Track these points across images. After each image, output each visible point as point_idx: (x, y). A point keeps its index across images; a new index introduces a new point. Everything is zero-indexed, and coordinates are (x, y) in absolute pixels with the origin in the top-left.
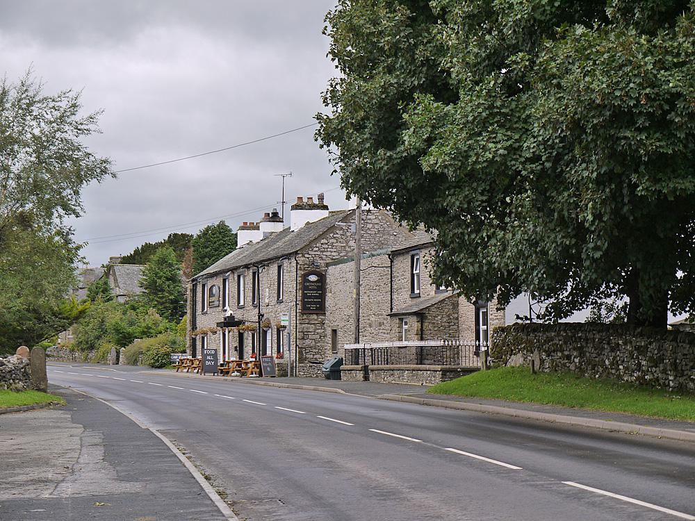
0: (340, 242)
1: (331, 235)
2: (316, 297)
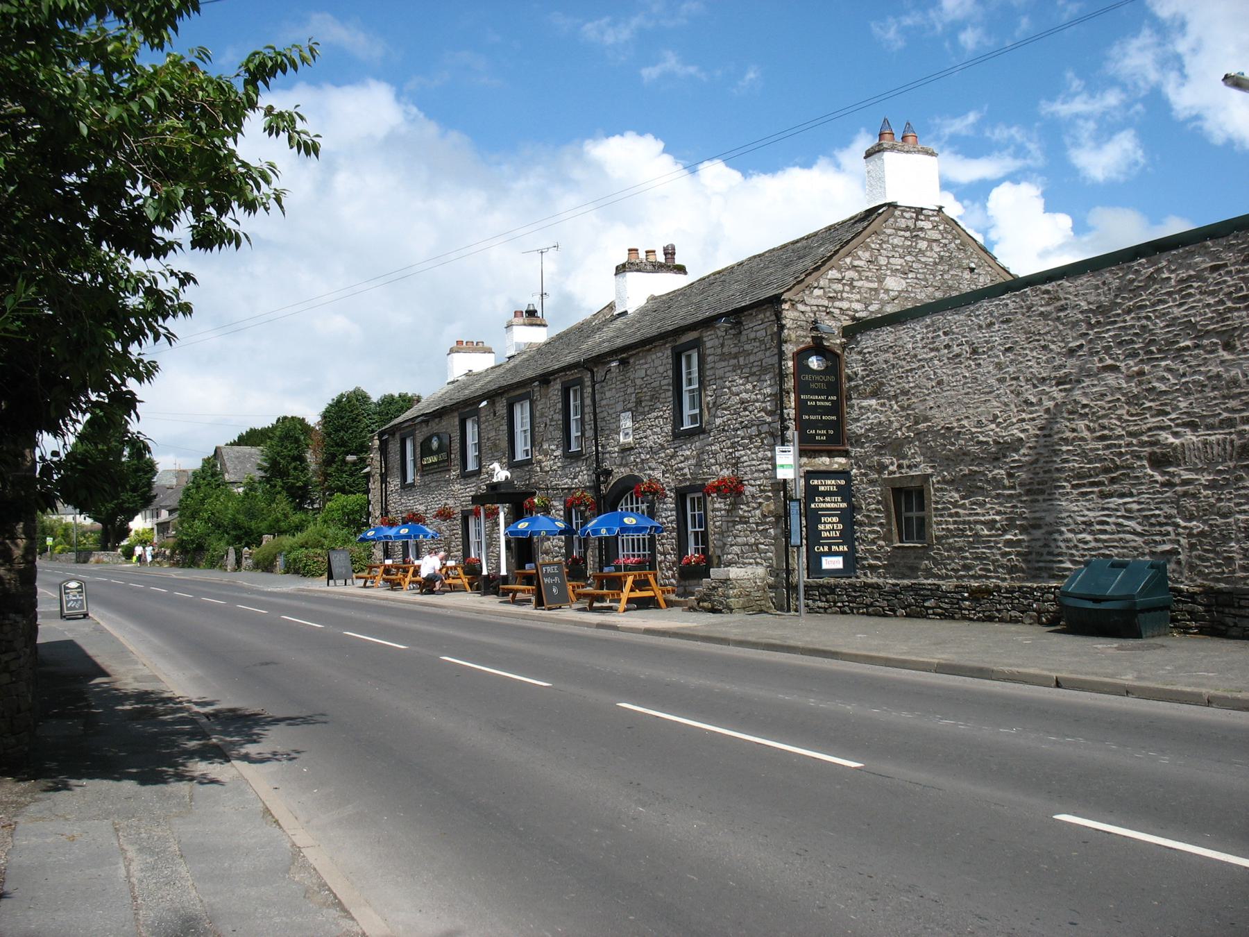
0: (867, 278)
1: (848, 260)
2: (826, 410)
